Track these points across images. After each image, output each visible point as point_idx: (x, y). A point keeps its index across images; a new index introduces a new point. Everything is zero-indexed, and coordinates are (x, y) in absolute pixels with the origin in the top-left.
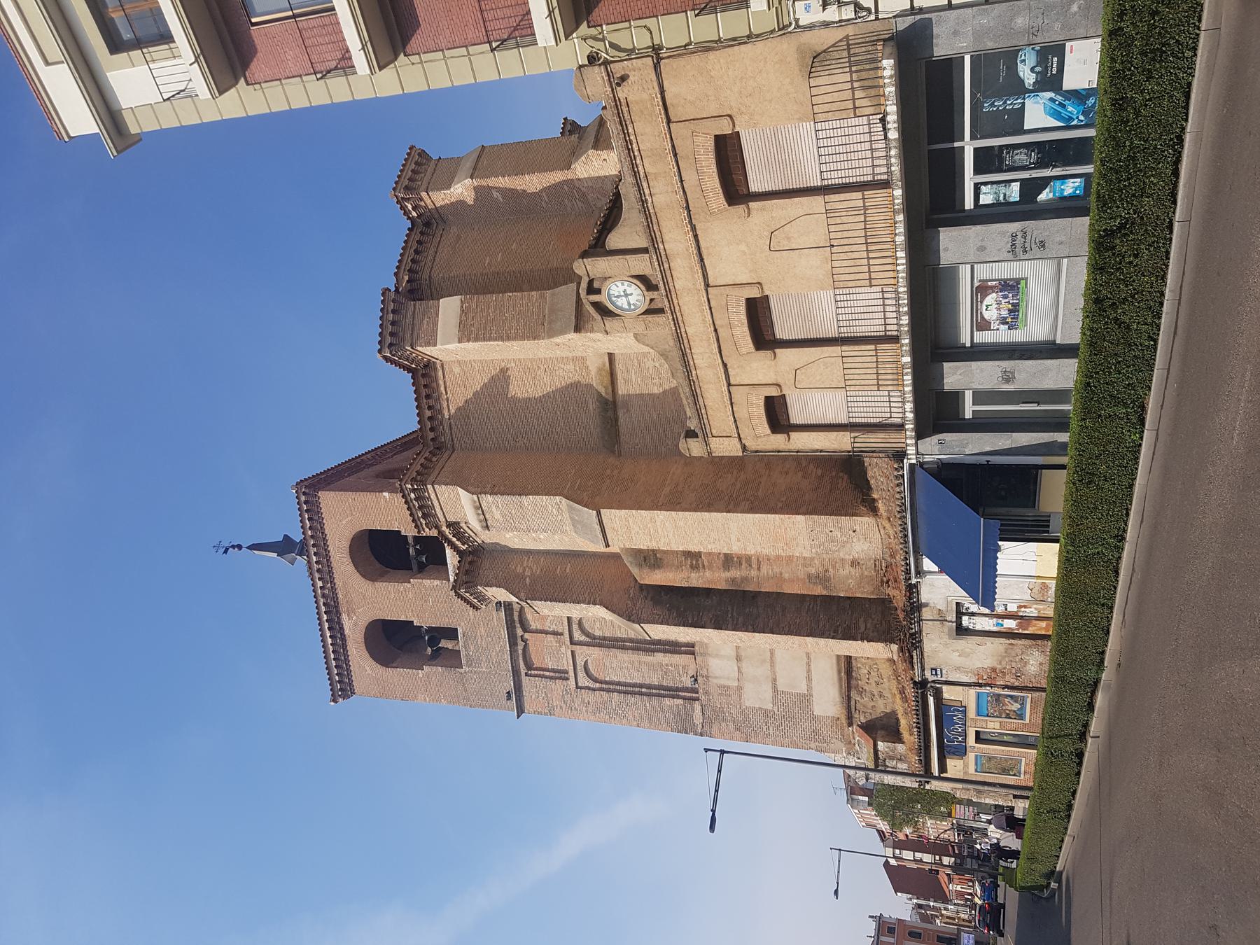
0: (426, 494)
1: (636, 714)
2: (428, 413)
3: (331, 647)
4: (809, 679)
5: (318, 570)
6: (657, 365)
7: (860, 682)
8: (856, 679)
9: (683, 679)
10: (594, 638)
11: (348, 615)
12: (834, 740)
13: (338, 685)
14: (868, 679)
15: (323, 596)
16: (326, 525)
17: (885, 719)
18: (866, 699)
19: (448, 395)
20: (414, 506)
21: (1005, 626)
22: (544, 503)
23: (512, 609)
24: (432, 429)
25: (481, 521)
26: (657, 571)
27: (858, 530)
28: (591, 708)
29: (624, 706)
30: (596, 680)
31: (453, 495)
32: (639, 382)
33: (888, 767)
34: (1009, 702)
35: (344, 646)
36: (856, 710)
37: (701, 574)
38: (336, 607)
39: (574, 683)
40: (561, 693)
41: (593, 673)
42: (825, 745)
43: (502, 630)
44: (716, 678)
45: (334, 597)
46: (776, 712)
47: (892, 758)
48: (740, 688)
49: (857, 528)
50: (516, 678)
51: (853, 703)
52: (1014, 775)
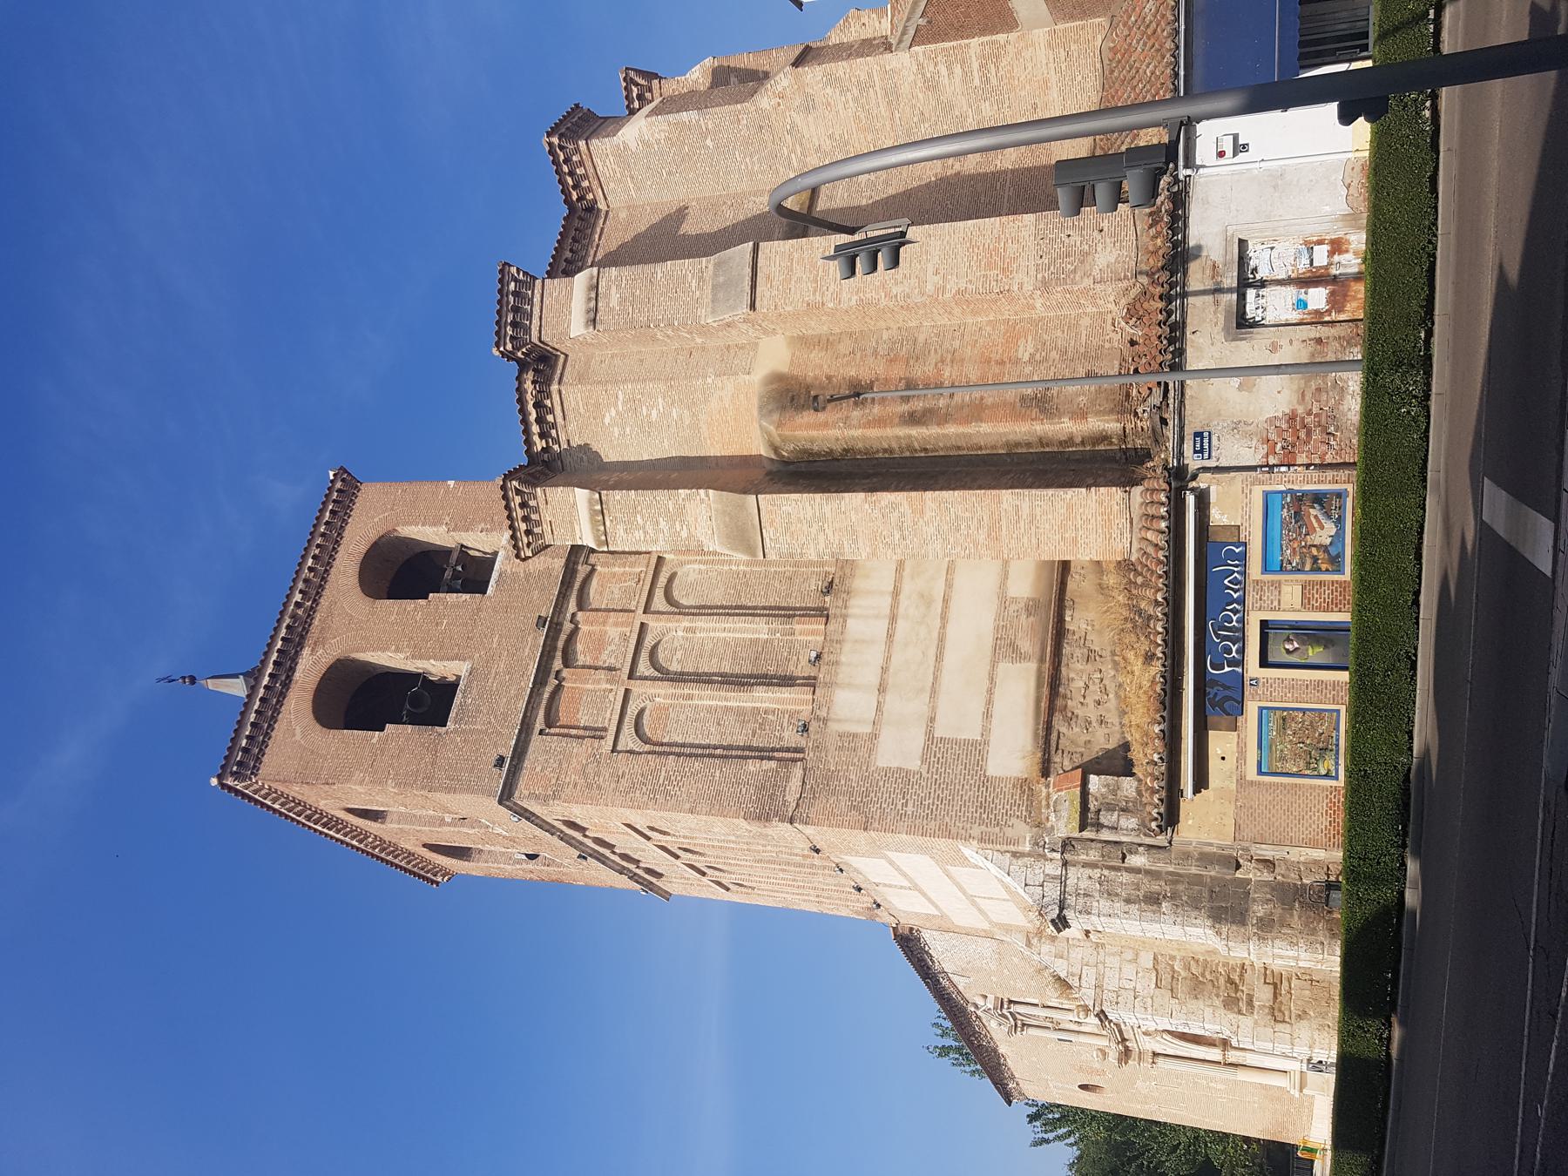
0: (530, 292)
2: (568, 254)
3: (262, 691)
5: (306, 581)
7: (1069, 701)
8: (1065, 697)
10: (668, 672)
12: (1014, 820)
14: (1084, 697)
15: (294, 616)
16: (349, 525)
17: (1105, 762)
18: (1076, 730)
19: (601, 242)
20: (508, 303)
21: (1311, 307)
22: (684, 272)
23: (560, 630)
27: (1106, 229)
29: (679, 778)
30: (646, 741)
31: (564, 293)
32: (845, 197)
34: (1316, 517)
36: (1057, 749)
37: (868, 411)
38: (302, 637)
39: (612, 744)
40: (584, 762)
41: (647, 730)
42: (997, 829)
43: (532, 663)
44: (839, 721)
45: (306, 622)
46: (924, 774)
47: (1111, 808)
48: (874, 736)
50: (523, 735)
51: (1054, 736)
52: (1327, 776)
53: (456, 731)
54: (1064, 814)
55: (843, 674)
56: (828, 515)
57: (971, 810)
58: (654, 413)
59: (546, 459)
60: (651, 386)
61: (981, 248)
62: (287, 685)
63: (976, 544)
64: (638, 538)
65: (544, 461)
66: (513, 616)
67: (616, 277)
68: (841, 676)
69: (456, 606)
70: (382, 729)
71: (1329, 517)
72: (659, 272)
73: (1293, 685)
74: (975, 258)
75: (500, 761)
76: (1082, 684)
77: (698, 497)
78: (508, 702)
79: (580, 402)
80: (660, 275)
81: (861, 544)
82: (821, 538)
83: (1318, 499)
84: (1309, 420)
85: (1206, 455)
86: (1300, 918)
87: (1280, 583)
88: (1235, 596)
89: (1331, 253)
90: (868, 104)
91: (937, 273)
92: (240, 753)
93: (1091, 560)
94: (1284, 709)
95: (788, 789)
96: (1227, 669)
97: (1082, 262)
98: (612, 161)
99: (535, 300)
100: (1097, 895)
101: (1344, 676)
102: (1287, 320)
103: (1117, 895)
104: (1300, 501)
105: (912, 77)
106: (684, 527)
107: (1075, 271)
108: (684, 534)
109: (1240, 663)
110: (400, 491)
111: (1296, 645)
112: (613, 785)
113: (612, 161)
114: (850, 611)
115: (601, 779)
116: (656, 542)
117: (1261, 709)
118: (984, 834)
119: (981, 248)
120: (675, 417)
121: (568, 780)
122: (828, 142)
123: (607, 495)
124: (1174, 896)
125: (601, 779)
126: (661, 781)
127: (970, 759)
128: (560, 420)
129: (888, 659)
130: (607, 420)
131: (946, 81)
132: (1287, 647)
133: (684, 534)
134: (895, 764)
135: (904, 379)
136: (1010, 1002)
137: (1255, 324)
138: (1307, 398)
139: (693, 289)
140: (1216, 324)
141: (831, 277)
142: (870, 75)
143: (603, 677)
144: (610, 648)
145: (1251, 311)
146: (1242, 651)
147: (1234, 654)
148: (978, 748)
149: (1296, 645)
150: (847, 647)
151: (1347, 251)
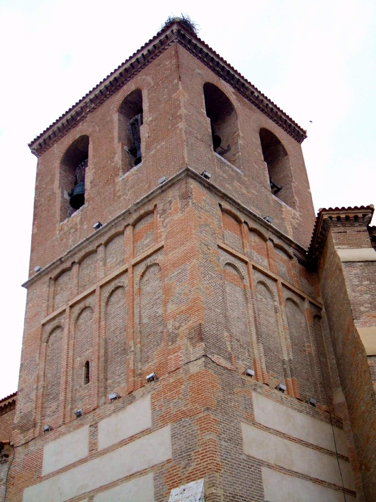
62: (218, 73)
64: (353, 280)
92: (189, 38)
118: (220, 498)
127: (254, 492)
133: (362, 309)
144: (260, 258)
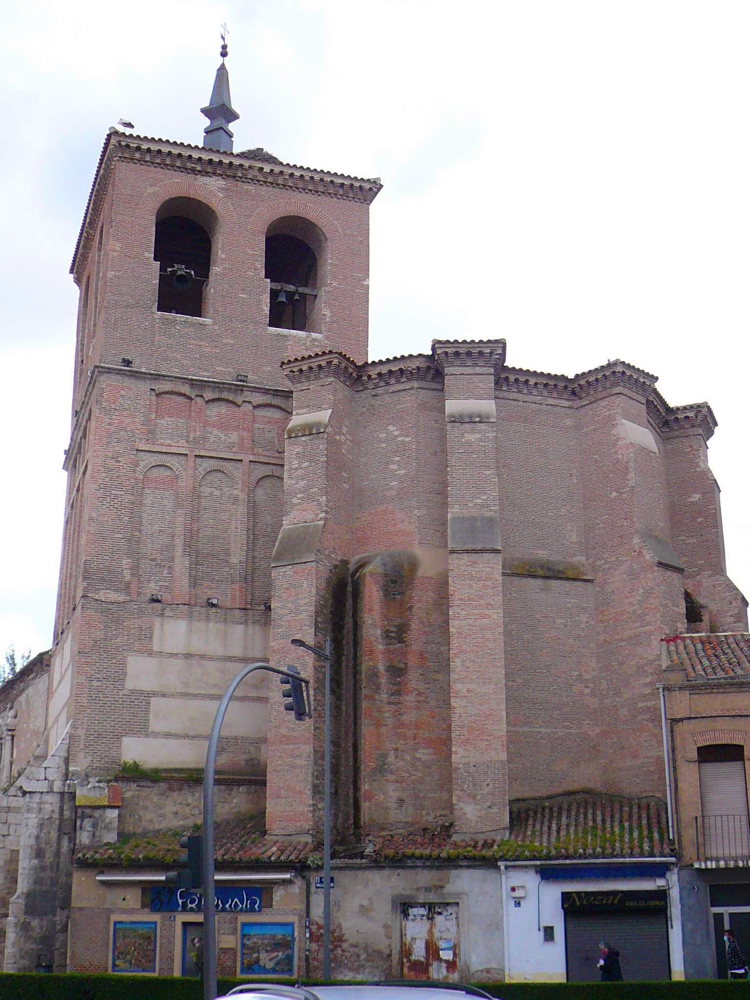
1: (105, 519)
2: (532, 381)
4: (168, 735)
6: (583, 626)
9: (152, 585)
11: (222, 189)
12: (90, 758)
13: (135, 145)
22: (489, 492)
24: (517, 380)
25: (461, 416)
26: (381, 593)
27: (491, 811)
28: (111, 463)
31: (482, 392)
33: (82, 821)
34: (277, 956)
35: (183, 169)
40: (129, 429)
42: (82, 747)
44: (162, 625)
47: (95, 826)
48: (150, 653)
49: (495, 810)
53: (154, 320)
54: (92, 794)
55: (200, 625)
56: (300, 617)
57: (96, 727)
58: (394, 467)
59: (363, 378)
60: (414, 464)
61: (485, 722)
63: (278, 727)
65: (362, 376)
66: (249, 352)
67: (487, 437)
68: (198, 623)
69: (259, 302)
70: (155, 259)
71: (277, 964)
72: (490, 472)
73: (171, 943)
74: (478, 718)
75: (128, 363)
76: (189, 801)
77: (319, 512)
78: (177, 360)
79: (404, 406)
80: (487, 473)
81: (281, 641)
82: (286, 611)
83: (289, 959)
84: (339, 950)
85: (319, 885)
86: (32, 949)
87: (236, 934)
88: (227, 906)
89: (447, 962)
90: (632, 621)
91: (468, 691)
93: (265, 808)
94: (156, 938)
95: (109, 591)
96: (180, 901)
97: (468, 795)
98: (606, 414)
99: (477, 368)
100: (41, 816)
101: (177, 974)
102: (406, 935)
103: (41, 830)
104: (286, 944)
105: (645, 656)
106: (299, 501)
107: (462, 790)
108: (295, 501)
109: (184, 909)
110: (361, 239)
111: (197, 945)
112: (110, 454)
113: (606, 414)
114: (250, 627)
115: (114, 444)
116: (290, 478)
117: (155, 923)
119: (485, 722)
120: (391, 484)
121: (114, 417)
122: (610, 590)
123: (323, 438)
124: (43, 868)
125: (114, 444)
126: (113, 492)
128: (393, 389)
129: (212, 659)
130: (391, 428)
131: (642, 682)
132: (196, 939)
133: (295, 501)
134: (129, 670)
135: (406, 666)
136: (13, 737)
137: (406, 915)
138: (353, 949)
139: (475, 501)
140: (403, 889)
141: (472, 611)
142: (649, 624)
143: (198, 433)
145: (413, 911)
146: (192, 910)
147: (190, 906)
148: (143, 730)
149: (197, 945)
150: (221, 626)
151: (448, 972)
